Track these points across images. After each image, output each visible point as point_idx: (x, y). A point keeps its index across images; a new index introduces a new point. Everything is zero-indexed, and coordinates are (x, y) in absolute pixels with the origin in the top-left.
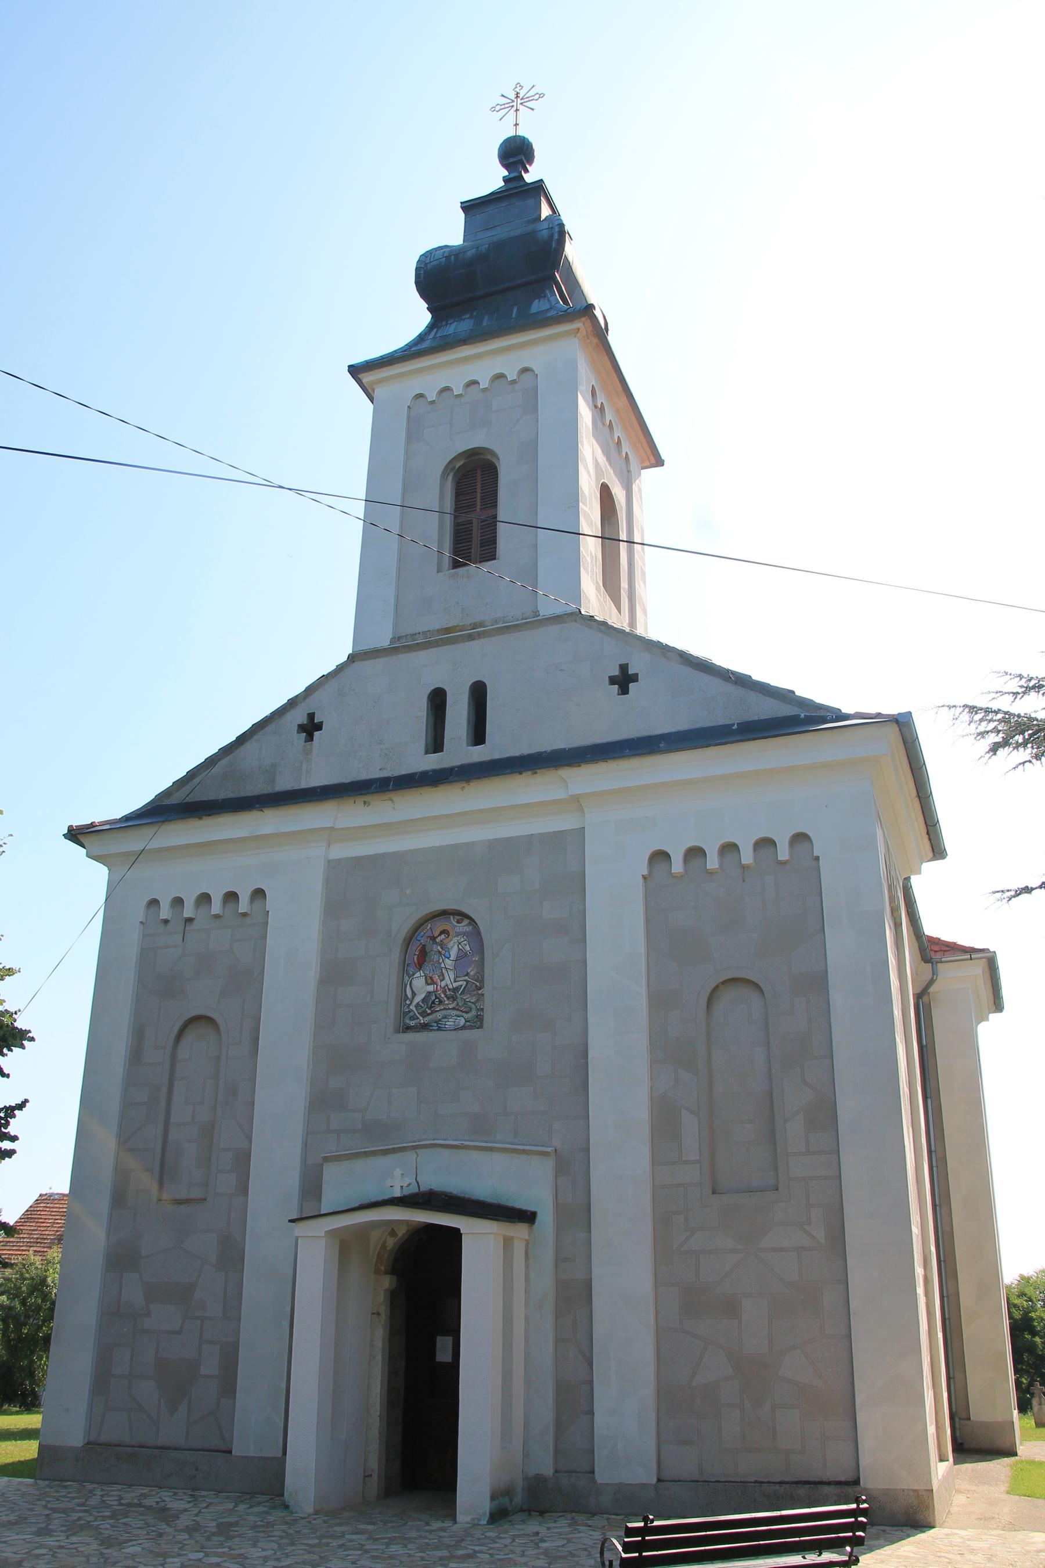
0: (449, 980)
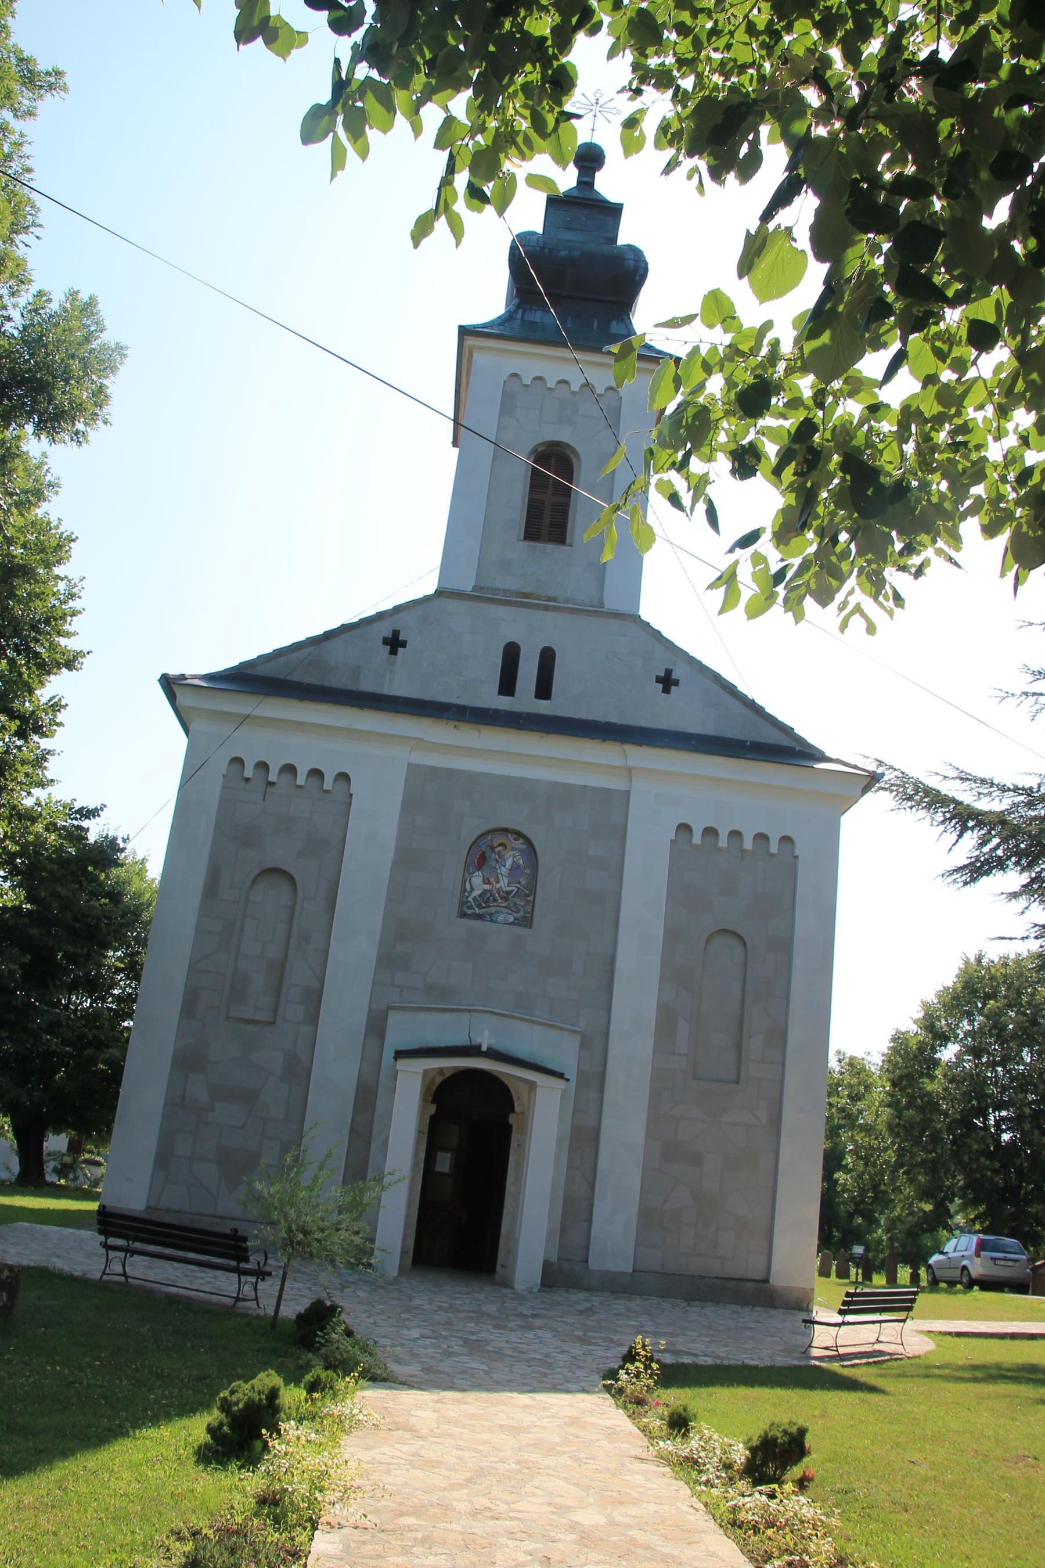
0: (503, 884)
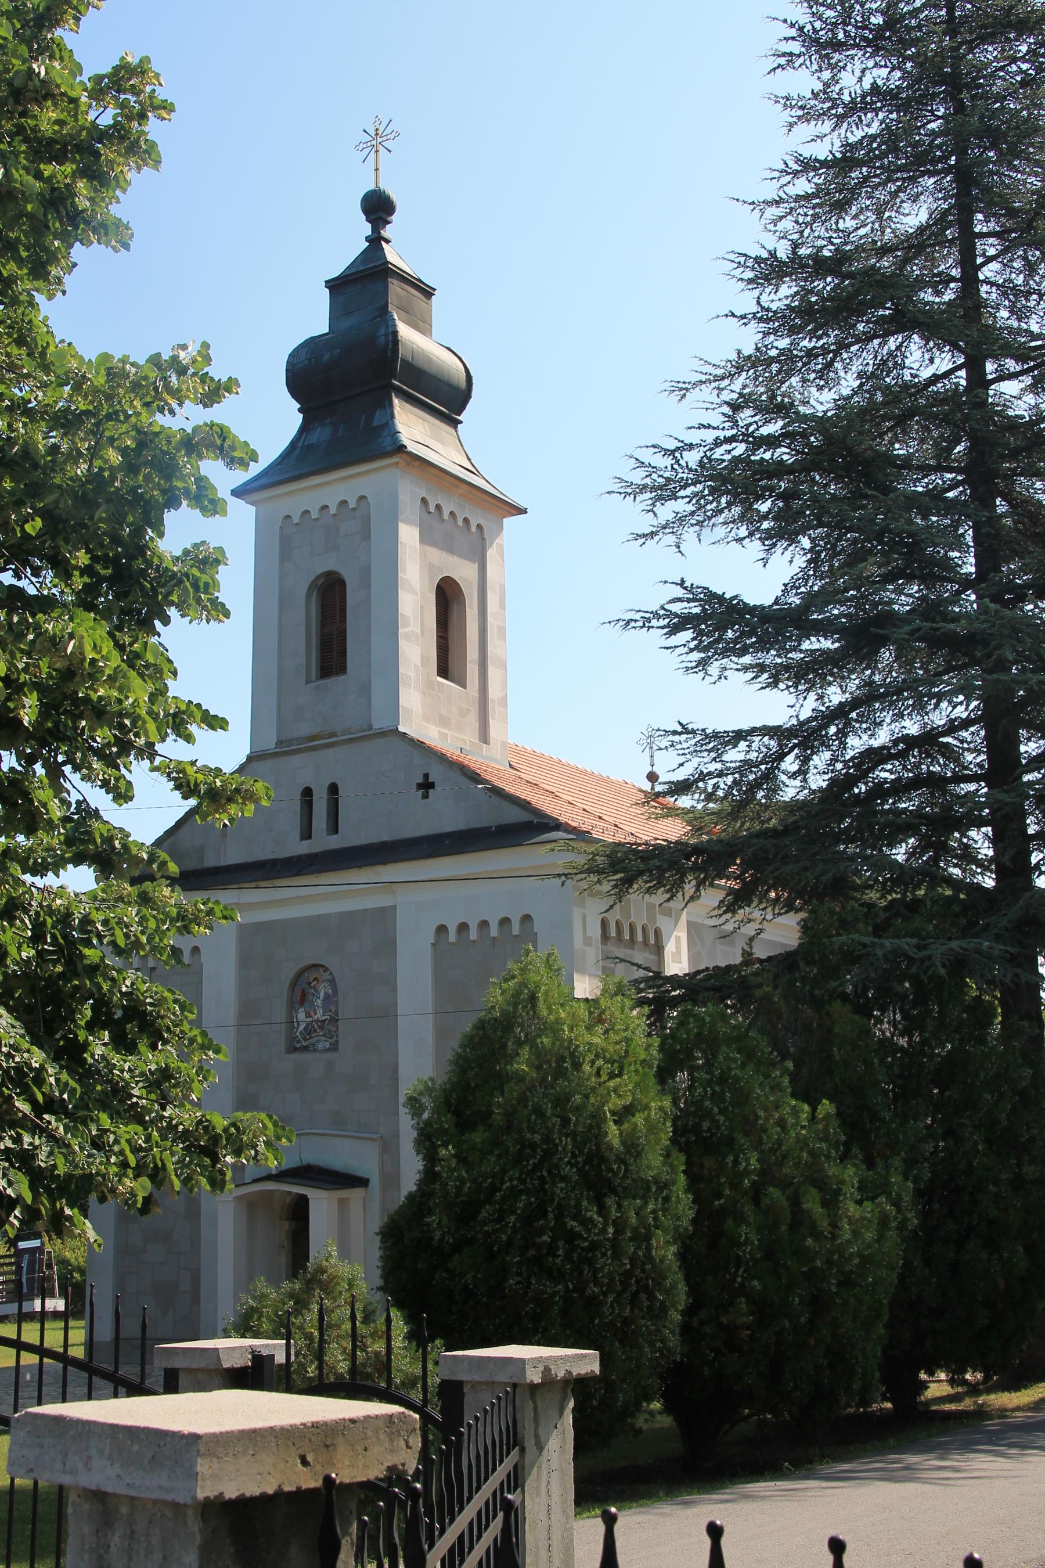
0: (319, 1015)
